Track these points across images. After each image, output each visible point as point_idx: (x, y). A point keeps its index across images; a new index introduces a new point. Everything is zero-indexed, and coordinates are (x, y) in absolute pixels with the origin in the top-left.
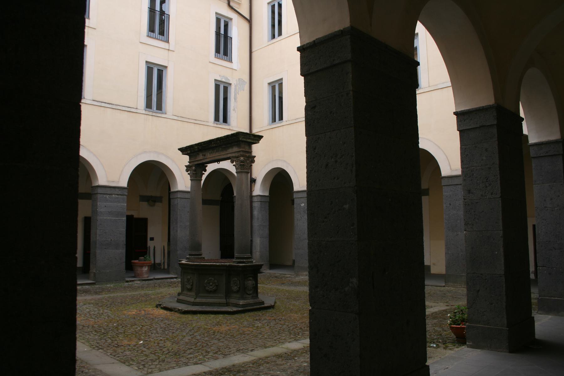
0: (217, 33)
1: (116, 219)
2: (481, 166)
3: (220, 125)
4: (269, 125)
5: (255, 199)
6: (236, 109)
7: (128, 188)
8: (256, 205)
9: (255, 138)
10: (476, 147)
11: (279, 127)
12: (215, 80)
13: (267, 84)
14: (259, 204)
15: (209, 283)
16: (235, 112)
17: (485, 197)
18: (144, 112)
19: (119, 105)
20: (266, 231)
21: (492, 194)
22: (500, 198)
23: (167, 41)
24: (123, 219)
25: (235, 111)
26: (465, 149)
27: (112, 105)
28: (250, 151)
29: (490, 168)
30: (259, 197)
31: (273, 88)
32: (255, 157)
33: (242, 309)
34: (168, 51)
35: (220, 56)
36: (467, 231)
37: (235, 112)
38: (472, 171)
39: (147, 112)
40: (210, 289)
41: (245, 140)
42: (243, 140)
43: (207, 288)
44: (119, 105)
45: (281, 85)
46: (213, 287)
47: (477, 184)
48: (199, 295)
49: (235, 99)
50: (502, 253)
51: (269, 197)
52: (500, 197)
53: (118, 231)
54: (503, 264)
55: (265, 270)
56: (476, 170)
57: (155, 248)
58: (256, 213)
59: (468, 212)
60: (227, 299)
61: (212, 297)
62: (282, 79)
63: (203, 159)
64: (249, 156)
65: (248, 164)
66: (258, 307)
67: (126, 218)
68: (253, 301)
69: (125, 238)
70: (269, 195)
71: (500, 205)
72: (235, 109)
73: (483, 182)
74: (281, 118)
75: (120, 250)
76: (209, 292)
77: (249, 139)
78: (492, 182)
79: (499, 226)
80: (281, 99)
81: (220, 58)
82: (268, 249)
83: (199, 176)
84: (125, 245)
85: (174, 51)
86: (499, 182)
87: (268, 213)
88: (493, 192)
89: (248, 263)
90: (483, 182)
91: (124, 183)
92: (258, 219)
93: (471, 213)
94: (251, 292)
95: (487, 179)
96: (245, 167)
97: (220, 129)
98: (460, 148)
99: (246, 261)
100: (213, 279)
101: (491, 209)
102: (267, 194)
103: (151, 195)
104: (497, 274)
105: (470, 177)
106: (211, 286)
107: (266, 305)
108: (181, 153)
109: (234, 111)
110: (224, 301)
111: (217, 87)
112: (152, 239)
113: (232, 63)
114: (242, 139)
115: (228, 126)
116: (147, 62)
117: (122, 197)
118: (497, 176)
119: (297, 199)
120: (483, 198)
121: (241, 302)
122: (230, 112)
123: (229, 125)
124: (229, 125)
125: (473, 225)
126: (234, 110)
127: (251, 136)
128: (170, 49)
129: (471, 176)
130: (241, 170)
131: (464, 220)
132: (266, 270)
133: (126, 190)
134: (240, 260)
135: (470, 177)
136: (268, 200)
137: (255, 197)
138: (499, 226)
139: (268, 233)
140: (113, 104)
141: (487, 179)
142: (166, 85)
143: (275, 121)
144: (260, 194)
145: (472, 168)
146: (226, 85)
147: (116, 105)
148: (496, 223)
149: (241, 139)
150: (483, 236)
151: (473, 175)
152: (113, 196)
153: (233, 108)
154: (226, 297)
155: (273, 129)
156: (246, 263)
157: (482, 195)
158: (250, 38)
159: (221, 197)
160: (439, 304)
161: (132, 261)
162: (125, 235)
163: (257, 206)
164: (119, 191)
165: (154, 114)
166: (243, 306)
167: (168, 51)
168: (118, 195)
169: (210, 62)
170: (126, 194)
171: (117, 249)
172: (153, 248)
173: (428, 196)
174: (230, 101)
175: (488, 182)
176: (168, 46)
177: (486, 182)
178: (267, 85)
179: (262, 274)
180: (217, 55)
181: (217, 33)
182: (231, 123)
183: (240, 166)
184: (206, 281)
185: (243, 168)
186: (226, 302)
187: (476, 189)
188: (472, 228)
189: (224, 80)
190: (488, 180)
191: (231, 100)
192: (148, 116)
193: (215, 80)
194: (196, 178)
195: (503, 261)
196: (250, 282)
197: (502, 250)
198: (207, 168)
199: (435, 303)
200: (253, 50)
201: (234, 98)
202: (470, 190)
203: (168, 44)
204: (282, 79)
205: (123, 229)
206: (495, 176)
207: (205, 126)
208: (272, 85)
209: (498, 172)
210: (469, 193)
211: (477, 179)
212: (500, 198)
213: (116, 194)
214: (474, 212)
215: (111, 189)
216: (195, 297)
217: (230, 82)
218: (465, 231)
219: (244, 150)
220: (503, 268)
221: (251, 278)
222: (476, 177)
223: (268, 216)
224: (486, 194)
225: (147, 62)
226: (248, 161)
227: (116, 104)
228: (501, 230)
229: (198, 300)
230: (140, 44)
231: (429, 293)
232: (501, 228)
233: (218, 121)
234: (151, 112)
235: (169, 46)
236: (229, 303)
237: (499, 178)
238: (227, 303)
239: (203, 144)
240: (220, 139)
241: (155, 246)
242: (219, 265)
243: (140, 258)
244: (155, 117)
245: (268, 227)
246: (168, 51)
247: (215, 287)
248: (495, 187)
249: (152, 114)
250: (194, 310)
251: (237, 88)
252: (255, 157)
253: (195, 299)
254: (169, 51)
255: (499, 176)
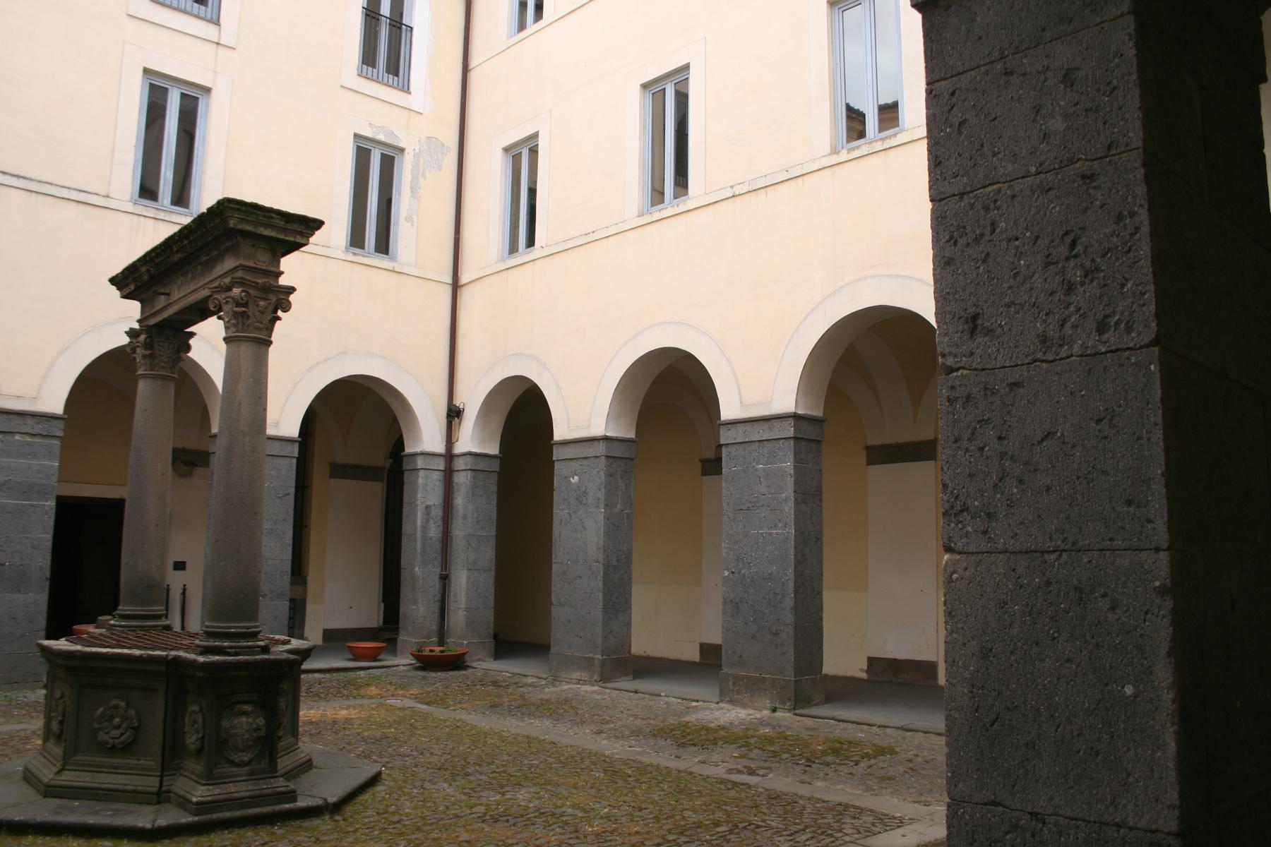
0: (369, 13)
1: (23, 505)
2: (1038, 173)
3: (364, 256)
4: (503, 260)
5: (459, 464)
6: (415, 218)
7: (66, 416)
8: (461, 479)
9: (289, 226)
10: (1008, 73)
11: (524, 265)
12: (356, 136)
13: (639, 86)
14: (469, 477)
15: (111, 718)
16: (413, 225)
17: (1064, 352)
18: (130, 207)
19: (51, 184)
20: (488, 553)
21: (1102, 327)
22: (1155, 350)
23: (216, 22)
24: (44, 505)
25: (410, 223)
26: (953, 94)
27: (25, 181)
28: (273, 269)
29: (1088, 178)
30: (469, 459)
31: (516, 160)
32: (292, 290)
33: (196, 819)
34: (217, 49)
35: (375, 74)
36: (960, 553)
37: (413, 225)
38: (986, 209)
39: (140, 207)
40: (112, 741)
41: (248, 228)
42: (240, 227)
43: (102, 736)
44: (51, 184)
45: (534, 152)
46: (122, 734)
47: (1016, 274)
48: (77, 758)
49: (414, 190)
50: (1167, 697)
51: (499, 460)
52: (1153, 343)
53: (27, 538)
54: (1171, 765)
55: (479, 660)
56: (1013, 197)
57: (187, 591)
58: (459, 501)
59: (965, 444)
60: (165, 778)
61: (116, 768)
62: (686, 67)
63: (170, 304)
64: (264, 284)
65: (262, 313)
66: (237, 813)
67: (54, 504)
68: (250, 788)
69: (49, 558)
70: (500, 453)
71: (1157, 392)
72: (411, 217)
73: (1047, 265)
74: (531, 242)
75: (31, 594)
76: (112, 750)
77: (267, 226)
78: (1104, 256)
79: (1149, 521)
80: (532, 192)
81: (375, 78)
82: (491, 603)
83: (162, 364)
84: (47, 578)
85: (234, 49)
86: (1144, 250)
87: (495, 502)
88: (1106, 317)
89: (236, 654)
90: (1047, 265)
91: (54, 401)
92: (465, 517)
93: (981, 449)
94: (246, 757)
95: (1073, 244)
96: (249, 322)
97: (365, 267)
98: (923, 95)
99: (231, 647)
100: (123, 704)
101: (1099, 421)
102: (494, 449)
103: (184, 448)
104: (1131, 829)
105: (977, 240)
106: (118, 727)
107: (301, 803)
108: (118, 293)
109: (408, 222)
110: (151, 783)
111: (362, 157)
112: (180, 566)
113: (410, 93)
114: (235, 224)
115: (392, 261)
116: (146, 71)
117: (46, 441)
118: (1132, 215)
119: (563, 463)
120: (1050, 357)
121: (199, 793)
122: (397, 223)
123: (393, 259)
124: (393, 259)
125: (989, 515)
126: (409, 219)
127: (274, 215)
128: (222, 42)
129: (982, 235)
130: (237, 331)
131: (945, 486)
132: (484, 661)
133: (61, 424)
134: (212, 643)
135: (977, 240)
136: (496, 466)
137: (461, 458)
138: (1149, 521)
139: (494, 557)
140: (31, 180)
141: (1073, 244)
142: (204, 138)
143: (862, 135)
144: (473, 450)
145: (990, 188)
146: (389, 152)
147: (40, 182)
148: (1129, 503)
149: (232, 224)
150: (1048, 583)
151: (993, 231)
152: (17, 437)
153: (406, 215)
154: (162, 771)
155: (510, 271)
156: (229, 654)
157: (1043, 339)
158: (465, 33)
159: (391, 461)
160: (930, 808)
161: (75, 627)
162: (50, 551)
163: (465, 483)
164: (37, 423)
165: (161, 215)
166: (202, 807)
167: (215, 46)
168: (32, 435)
169: (342, 86)
170: (60, 434)
171: (19, 591)
172: (181, 591)
173: (933, 462)
174: (400, 194)
175: (1076, 256)
176: (218, 33)
177: (1067, 259)
178: (499, 152)
179: (464, 672)
180: (365, 70)
181: (369, 13)
182: (399, 256)
183: (235, 318)
184: (100, 710)
185: (243, 324)
186: (155, 790)
187: (1008, 305)
188: (985, 532)
189: (381, 137)
190: (1079, 248)
191: (402, 193)
192: (142, 218)
193: (356, 136)
194: (151, 370)
195: (1172, 747)
196: (244, 719)
197: (1164, 674)
198: (192, 342)
199: (919, 802)
200: (473, 62)
201: (411, 188)
202: (975, 317)
203: (217, 27)
204: (686, 67)
205: (45, 536)
206: (1120, 218)
207: (317, 257)
208: (513, 153)
209: (1141, 190)
210: (973, 332)
211: (1018, 247)
212: (1155, 350)
213: (26, 433)
214: (1000, 438)
215: (12, 417)
216: (59, 765)
217: (402, 145)
218: (948, 549)
219: (251, 264)
220: (1173, 796)
221: (248, 708)
222: (1009, 241)
223: (495, 510)
224: (1068, 330)
225: (146, 71)
226: (262, 303)
227: (40, 179)
228: (1157, 550)
229: (68, 778)
230: (129, 19)
231: (910, 761)
232: (1161, 533)
233: (362, 246)
234: (153, 211)
235: (220, 34)
236: (169, 792)
237: (1146, 229)
238: (159, 793)
239: (153, 254)
240: (186, 232)
241: (185, 585)
242: (141, 656)
243: (100, 618)
244: (166, 223)
245: (493, 541)
246: (217, 49)
247: (127, 734)
248: (1123, 285)
249: (156, 214)
250: (17, 819)
251: (422, 160)
252: (292, 290)
253: (59, 773)
254: (220, 47)
255: (1143, 217)
